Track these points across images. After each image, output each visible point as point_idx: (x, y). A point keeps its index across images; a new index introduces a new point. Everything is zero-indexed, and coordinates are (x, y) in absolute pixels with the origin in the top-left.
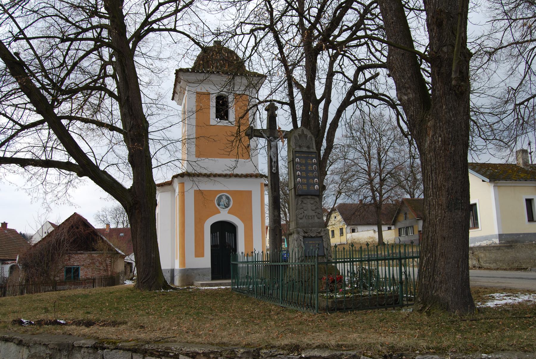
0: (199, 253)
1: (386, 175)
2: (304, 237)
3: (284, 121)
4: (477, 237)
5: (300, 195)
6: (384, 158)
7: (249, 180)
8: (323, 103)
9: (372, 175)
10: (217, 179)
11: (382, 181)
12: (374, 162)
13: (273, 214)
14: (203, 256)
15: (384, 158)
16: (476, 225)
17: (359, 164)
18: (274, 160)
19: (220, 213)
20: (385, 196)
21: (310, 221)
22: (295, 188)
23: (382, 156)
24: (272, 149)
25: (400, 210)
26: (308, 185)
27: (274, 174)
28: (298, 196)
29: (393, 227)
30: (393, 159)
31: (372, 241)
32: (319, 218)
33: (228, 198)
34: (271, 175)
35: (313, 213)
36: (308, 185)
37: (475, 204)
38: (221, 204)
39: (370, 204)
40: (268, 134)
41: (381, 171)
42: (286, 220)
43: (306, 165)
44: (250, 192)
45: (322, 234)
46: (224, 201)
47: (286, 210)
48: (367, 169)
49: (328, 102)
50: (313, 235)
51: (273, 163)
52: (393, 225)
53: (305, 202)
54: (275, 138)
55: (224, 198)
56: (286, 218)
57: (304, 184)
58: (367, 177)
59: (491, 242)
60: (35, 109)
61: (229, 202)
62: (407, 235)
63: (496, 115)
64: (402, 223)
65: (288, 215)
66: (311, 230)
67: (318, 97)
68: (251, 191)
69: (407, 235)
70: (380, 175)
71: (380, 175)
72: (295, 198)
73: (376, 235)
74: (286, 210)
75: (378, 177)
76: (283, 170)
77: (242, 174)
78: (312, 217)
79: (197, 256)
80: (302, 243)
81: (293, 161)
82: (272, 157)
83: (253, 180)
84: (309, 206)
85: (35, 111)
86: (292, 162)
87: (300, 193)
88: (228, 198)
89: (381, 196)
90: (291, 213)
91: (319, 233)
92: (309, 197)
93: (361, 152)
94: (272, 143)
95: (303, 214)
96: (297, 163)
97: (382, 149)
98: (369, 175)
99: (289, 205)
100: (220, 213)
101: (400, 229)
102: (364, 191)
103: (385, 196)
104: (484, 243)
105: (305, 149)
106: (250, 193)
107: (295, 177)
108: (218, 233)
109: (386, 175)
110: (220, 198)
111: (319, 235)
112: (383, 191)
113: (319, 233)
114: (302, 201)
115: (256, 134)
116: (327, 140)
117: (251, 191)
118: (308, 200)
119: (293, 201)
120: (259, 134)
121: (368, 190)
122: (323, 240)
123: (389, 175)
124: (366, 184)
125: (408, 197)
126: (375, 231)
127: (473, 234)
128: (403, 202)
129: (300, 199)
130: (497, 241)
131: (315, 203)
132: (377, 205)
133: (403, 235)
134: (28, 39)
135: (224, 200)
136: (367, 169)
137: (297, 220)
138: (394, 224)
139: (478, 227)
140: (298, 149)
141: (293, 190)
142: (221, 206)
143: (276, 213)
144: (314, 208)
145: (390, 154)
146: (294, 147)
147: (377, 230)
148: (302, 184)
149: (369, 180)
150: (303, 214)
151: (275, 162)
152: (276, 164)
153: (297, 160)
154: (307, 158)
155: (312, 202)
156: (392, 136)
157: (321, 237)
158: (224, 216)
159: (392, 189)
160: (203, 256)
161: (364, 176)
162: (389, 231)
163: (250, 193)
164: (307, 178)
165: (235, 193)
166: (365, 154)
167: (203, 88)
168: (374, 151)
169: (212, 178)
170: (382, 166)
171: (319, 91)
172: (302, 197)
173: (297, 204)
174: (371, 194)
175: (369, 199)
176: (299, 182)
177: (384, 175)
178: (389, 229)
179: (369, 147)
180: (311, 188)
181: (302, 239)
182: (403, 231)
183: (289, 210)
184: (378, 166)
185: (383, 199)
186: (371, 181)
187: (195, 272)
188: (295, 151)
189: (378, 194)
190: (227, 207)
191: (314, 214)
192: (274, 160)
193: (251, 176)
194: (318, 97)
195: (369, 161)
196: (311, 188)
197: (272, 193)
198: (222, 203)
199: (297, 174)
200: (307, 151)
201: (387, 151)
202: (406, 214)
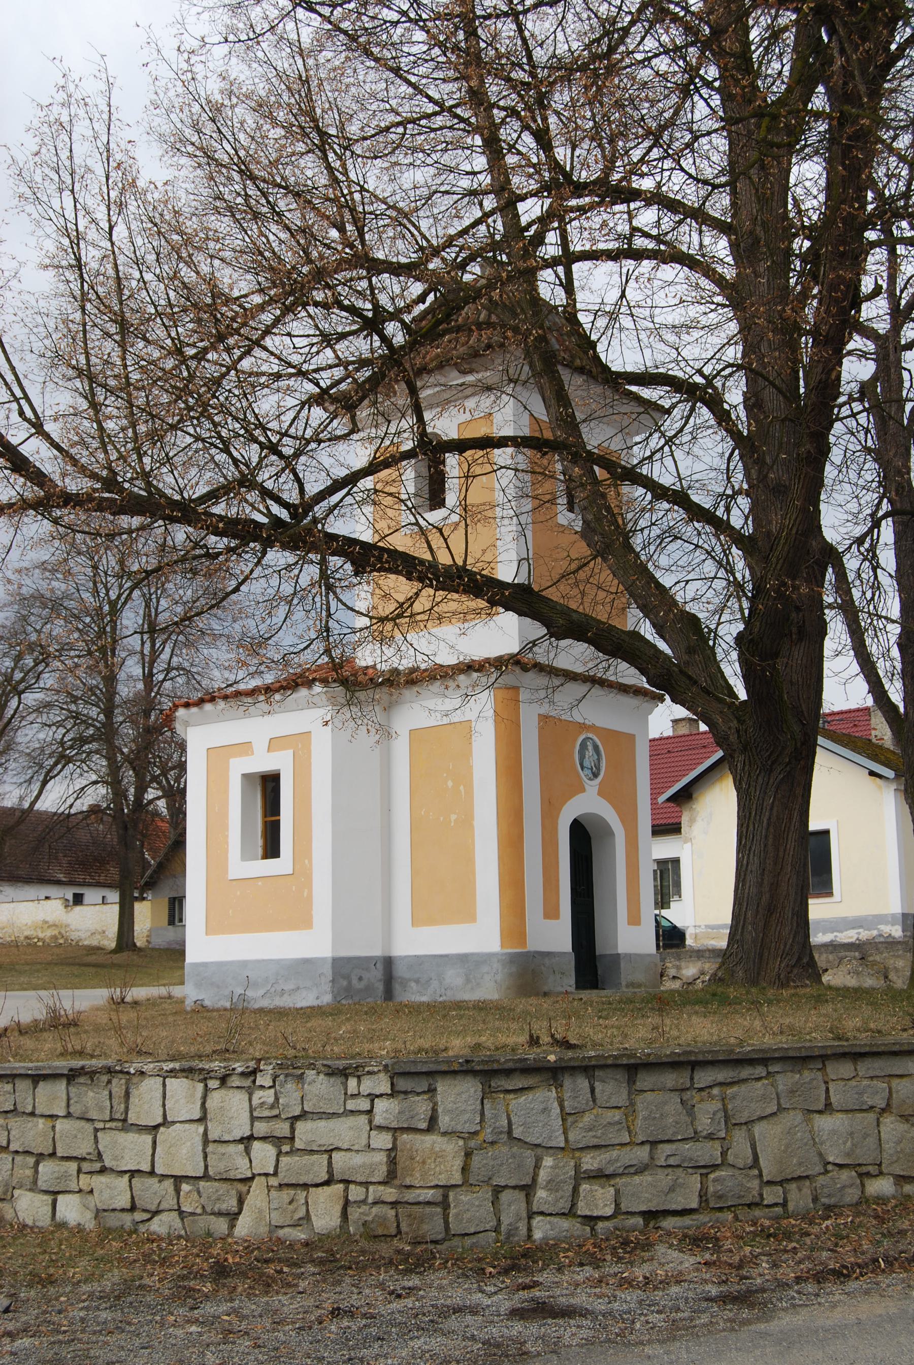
4: (824, 921)
16: (825, 888)
27: (142, 653)
31: (55, 938)
37: (826, 833)
59: (875, 933)
60: (729, 273)
61: (599, 760)
63: (502, 467)
79: (547, 916)
85: (719, 280)
104: (849, 936)
127: (817, 909)
130: (897, 932)
139: (830, 894)
162: (78, 909)
187: (547, 961)
190: (595, 775)
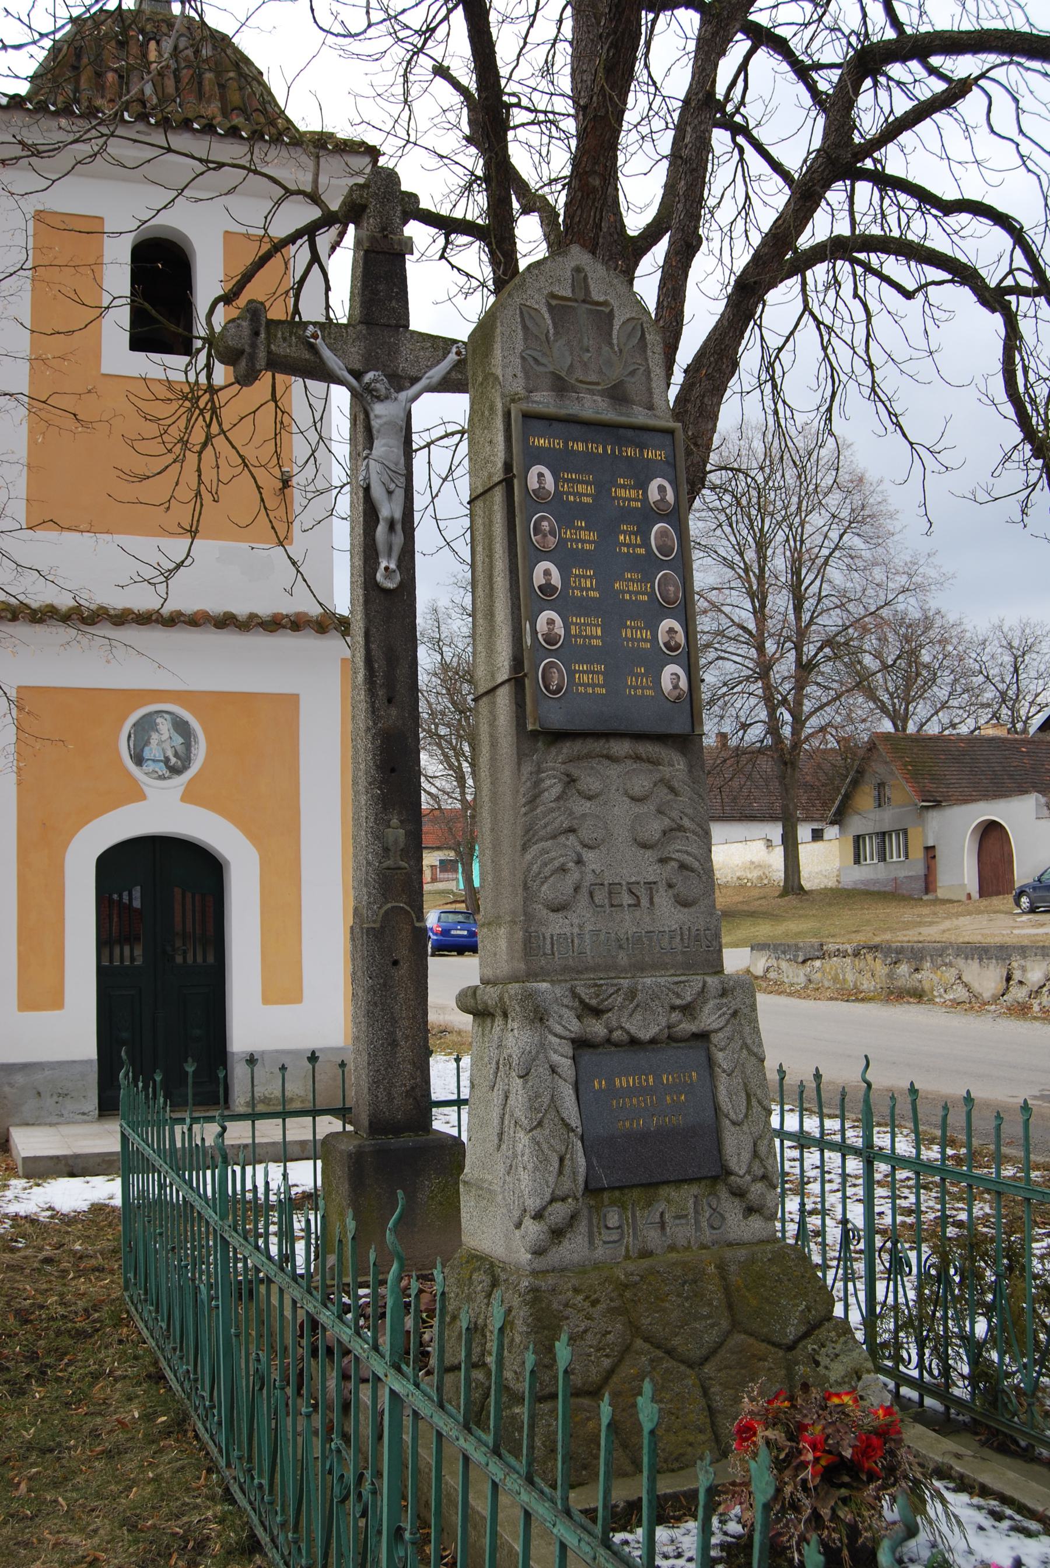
0: (39, 991)
1: (821, 649)
2: (581, 1044)
3: (444, 294)
5: (556, 737)
6: (814, 588)
7: (285, 641)
8: (660, 249)
9: (770, 646)
10: (130, 634)
11: (805, 668)
12: (779, 601)
13: (378, 836)
14: (55, 1000)
15: (814, 588)
17: (727, 609)
18: (385, 512)
19: (141, 796)
20: (814, 722)
21: (627, 924)
22: (517, 681)
23: (807, 582)
24: (379, 447)
25: (861, 772)
26: (616, 659)
28: (538, 737)
29: (831, 832)
30: (843, 593)
31: (760, 878)
32: (684, 903)
33: (182, 727)
34: (367, 602)
35: (644, 868)
36: (616, 659)
38: (147, 754)
39: (760, 751)
40: (355, 353)
41: (802, 634)
42: (463, 801)
44: (291, 701)
45: (709, 1019)
46: (163, 741)
47: (465, 765)
48: (752, 626)
49: (686, 249)
50: (645, 1026)
51: (381, 530)
52: (832, 823)
53: (589, 782)
54: (402, 381)
55: (164, 726)
56: (463, 793)
57: (588, 654)
58: (753, 653)
62: (883, 858)
64: (867, 819)
65: (470, 782)
66: (632, 994)
67: (635, 223)
68: (298, 695)
69: (883, 858)
70: (798, 648)
71: (798, 648)
72: (521, 756)
73: (777, 859)
74: (465, 765)
75: (792, 656)
76: (442, 585)
77: (252, 616)
78: (640, 894)
79: (28, 1002)
80: (567, 1092)
81: (508, 482)
82: (378, 492)
83: (307, 642)
84: (621, 811)
86: (498, 496)
87: (556, 718)
88: (182, 727)
89: (798, 722)
90: (484, 773)
91: (688, 1010)
92: (621, 748)
93: (731, 566)
94: (379, 409)
95: (573, 876)
96: (538, 500)
97: (806, 557)
98: (761, 648)
99: (473, 748)
100: (141, 796)
101: (858, 840)
102: (738, 705)
103: (814, 722)
105: (592, 406)
106: (288, 704)
107: (524, 601)
109: (821, 649)
110: (145, 727)
111: (687, 1027)
112: (807, 706)
113: (688, 1010)
114: (571, 780)
115: (281, 348)
117: (298, 695)
118: (613, 771)
119: (506, 774)
121: (753, 701)
122: (711, 1063)
123: (827, 650)
124: (748, 678)
125: (887, 726)
126: (769, 844)
128: (871, 747)
129: (555, 760)
131: (663, 792)
132: (784, 756)
133: (871, 860)
135: (165, 739)
136: (752, 626)
137: (529, 917)
138: (839, 819)
140: (544, 401)
141: (504, 698)
142: (149, 767)
143: (397, 834)
144: (654, 828)
145: (835, 574)
146: (518, 386)
147: (777, 839)
148: (571, 651)
149: (758, 665)
150: (573, 876)
151: (392, 525)
152: (398, 539)
153: (540, 477)
155: (641, 783)
156: (844, 514)
157: (703, 1037)
158: (163, 810)
159: (838, 697)
160: (55, 1000)
161: (743, 650)
162: (819, 845)
163: (288, 704)
164: (611, 610)
165: (214, 703)
166: (746, 570)
167: (74, 197)
168: (779, 563)
169: (106, 630)
170: (806, 617)
171: (641, 190)
172: (567, 749)
173: (533, 801)
174: (763, 715)
175: (756, 733)
176: (551, 639)
177: (809, 650)
178: (817, 835)
179: (761, 547)
180: (636, 684)
181: (565, 1064)
182: (870, 847)
183: (472, 765)
184: (791, 617)
185: (808, 731)
186: (764, 669)
187: (20, 1079)
188: (527, 416)
189: (788, 717)
191: (652, 872)
192: (388, 509)
193: (296, 624)
194: (635, 223)
195: (759, 598)
196: (636, 684)
197: (373, 711)
198: (153, 751)
199: (539, 579)
200: (610, 415)
201: (826, 563)
202: (881, 786)
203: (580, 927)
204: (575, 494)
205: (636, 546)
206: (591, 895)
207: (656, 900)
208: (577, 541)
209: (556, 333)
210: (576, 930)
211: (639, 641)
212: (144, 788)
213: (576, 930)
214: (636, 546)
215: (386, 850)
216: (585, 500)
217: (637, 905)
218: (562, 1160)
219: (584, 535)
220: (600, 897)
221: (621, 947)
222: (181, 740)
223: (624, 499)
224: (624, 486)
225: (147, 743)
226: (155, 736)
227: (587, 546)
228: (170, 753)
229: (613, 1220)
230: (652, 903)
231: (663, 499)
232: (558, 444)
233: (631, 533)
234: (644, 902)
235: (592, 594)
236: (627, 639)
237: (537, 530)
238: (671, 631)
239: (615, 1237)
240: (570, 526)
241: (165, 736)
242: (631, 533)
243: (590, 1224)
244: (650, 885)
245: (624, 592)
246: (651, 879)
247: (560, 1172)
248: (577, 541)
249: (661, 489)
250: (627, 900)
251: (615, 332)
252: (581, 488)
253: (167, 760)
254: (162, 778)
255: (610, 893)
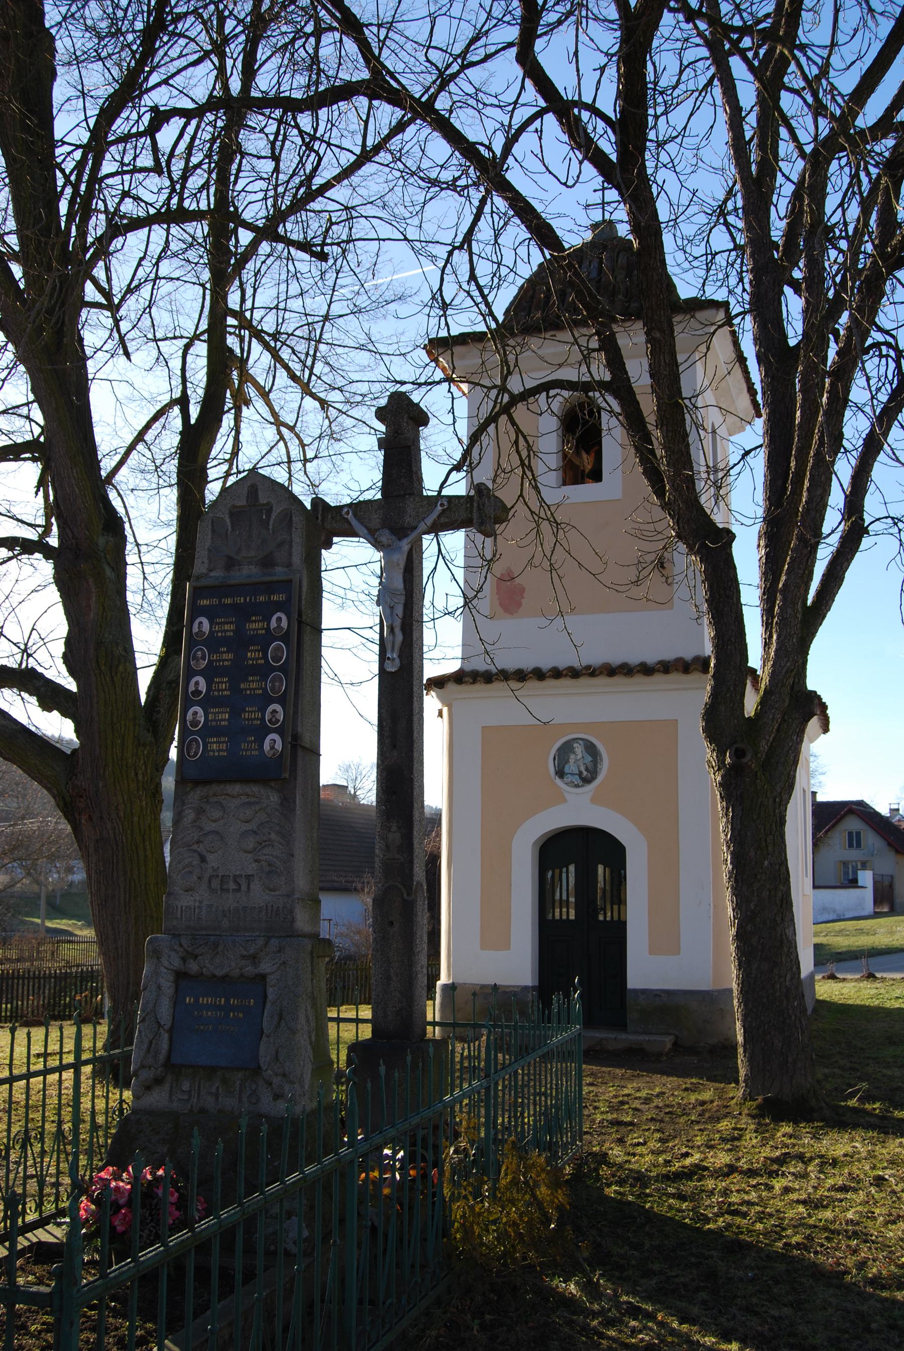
2: (180, 976)
38: (567, 770)
43: (240, 642)
46: (578, 759)
55: (579, 749)
88: (591, 749)
108: (572, 868)
116: (801, 500)
120: (451, 514)
134: (292, 334)
135: (578, 761)
142: (568, 779)
154: (243, 613)
157: (263, 977)
158: (578, 809)
160: (506, 945)
190: (587, 781)
191: (251, 868)
198: (571, 767)
203: (200, 902)
204: (221, 631)
205: (259, 659)
206: (210, 881)
207: (252, 886)
208: (219, 661)
209: (233, 529)
210: (197, 904)
211: (252, 720)
212: (566, 794)
213: (197, 904)
214: (259, 659)
215: (387, 847)
216: (228, 634)
217: (238, 890)
218: (151, 1042)
219: (225, 656)
220: (215, 883)
221: (225, 916)
222: (590, 759)
223: (254, 630)
224: (255, 621)
225: (567, 762)
226: (572, 757)
227: (226, 663)
228: (582, 769)
229: (186, 1086)
230: (249, 888)
231: (279, 626)
232: (215, 601)
233: (255, 651)
234: (244, 887)
235: (225, 693)
236: (245, 719)
237: (194, 658)
238: (274, 711)
239: (186, 1097)
240: (217, 652)
241: (579, 757)
242: (255, 651)
243: (171, 1087)
244: (249, 877)
245: (246, 689)
246: (250, 873)
247: (148, 1051)
248: (219, 661)
249: (279, 620)
250: (232, 886)
251: (272, 521)
252: (226, 627)
253: (580, 773)
254: (577, 786)
255: (222, 881)
